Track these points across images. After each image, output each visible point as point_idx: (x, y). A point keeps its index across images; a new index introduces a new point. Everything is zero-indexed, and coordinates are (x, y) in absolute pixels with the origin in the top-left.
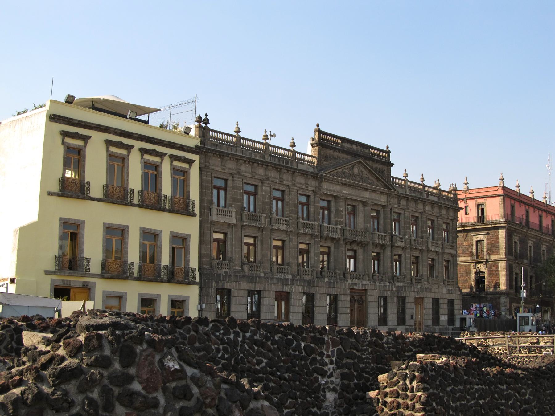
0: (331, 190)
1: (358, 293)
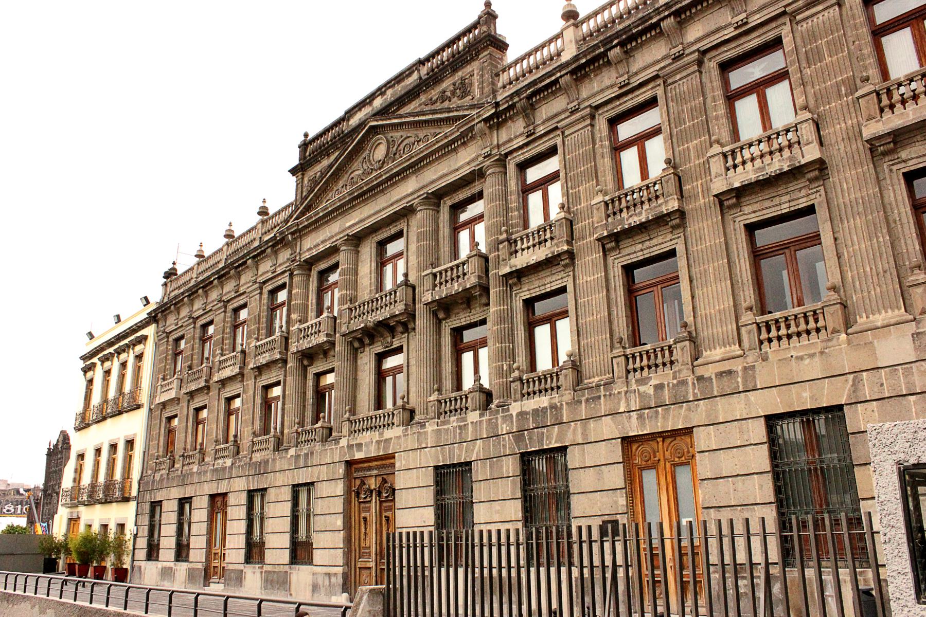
1: (378, 467)
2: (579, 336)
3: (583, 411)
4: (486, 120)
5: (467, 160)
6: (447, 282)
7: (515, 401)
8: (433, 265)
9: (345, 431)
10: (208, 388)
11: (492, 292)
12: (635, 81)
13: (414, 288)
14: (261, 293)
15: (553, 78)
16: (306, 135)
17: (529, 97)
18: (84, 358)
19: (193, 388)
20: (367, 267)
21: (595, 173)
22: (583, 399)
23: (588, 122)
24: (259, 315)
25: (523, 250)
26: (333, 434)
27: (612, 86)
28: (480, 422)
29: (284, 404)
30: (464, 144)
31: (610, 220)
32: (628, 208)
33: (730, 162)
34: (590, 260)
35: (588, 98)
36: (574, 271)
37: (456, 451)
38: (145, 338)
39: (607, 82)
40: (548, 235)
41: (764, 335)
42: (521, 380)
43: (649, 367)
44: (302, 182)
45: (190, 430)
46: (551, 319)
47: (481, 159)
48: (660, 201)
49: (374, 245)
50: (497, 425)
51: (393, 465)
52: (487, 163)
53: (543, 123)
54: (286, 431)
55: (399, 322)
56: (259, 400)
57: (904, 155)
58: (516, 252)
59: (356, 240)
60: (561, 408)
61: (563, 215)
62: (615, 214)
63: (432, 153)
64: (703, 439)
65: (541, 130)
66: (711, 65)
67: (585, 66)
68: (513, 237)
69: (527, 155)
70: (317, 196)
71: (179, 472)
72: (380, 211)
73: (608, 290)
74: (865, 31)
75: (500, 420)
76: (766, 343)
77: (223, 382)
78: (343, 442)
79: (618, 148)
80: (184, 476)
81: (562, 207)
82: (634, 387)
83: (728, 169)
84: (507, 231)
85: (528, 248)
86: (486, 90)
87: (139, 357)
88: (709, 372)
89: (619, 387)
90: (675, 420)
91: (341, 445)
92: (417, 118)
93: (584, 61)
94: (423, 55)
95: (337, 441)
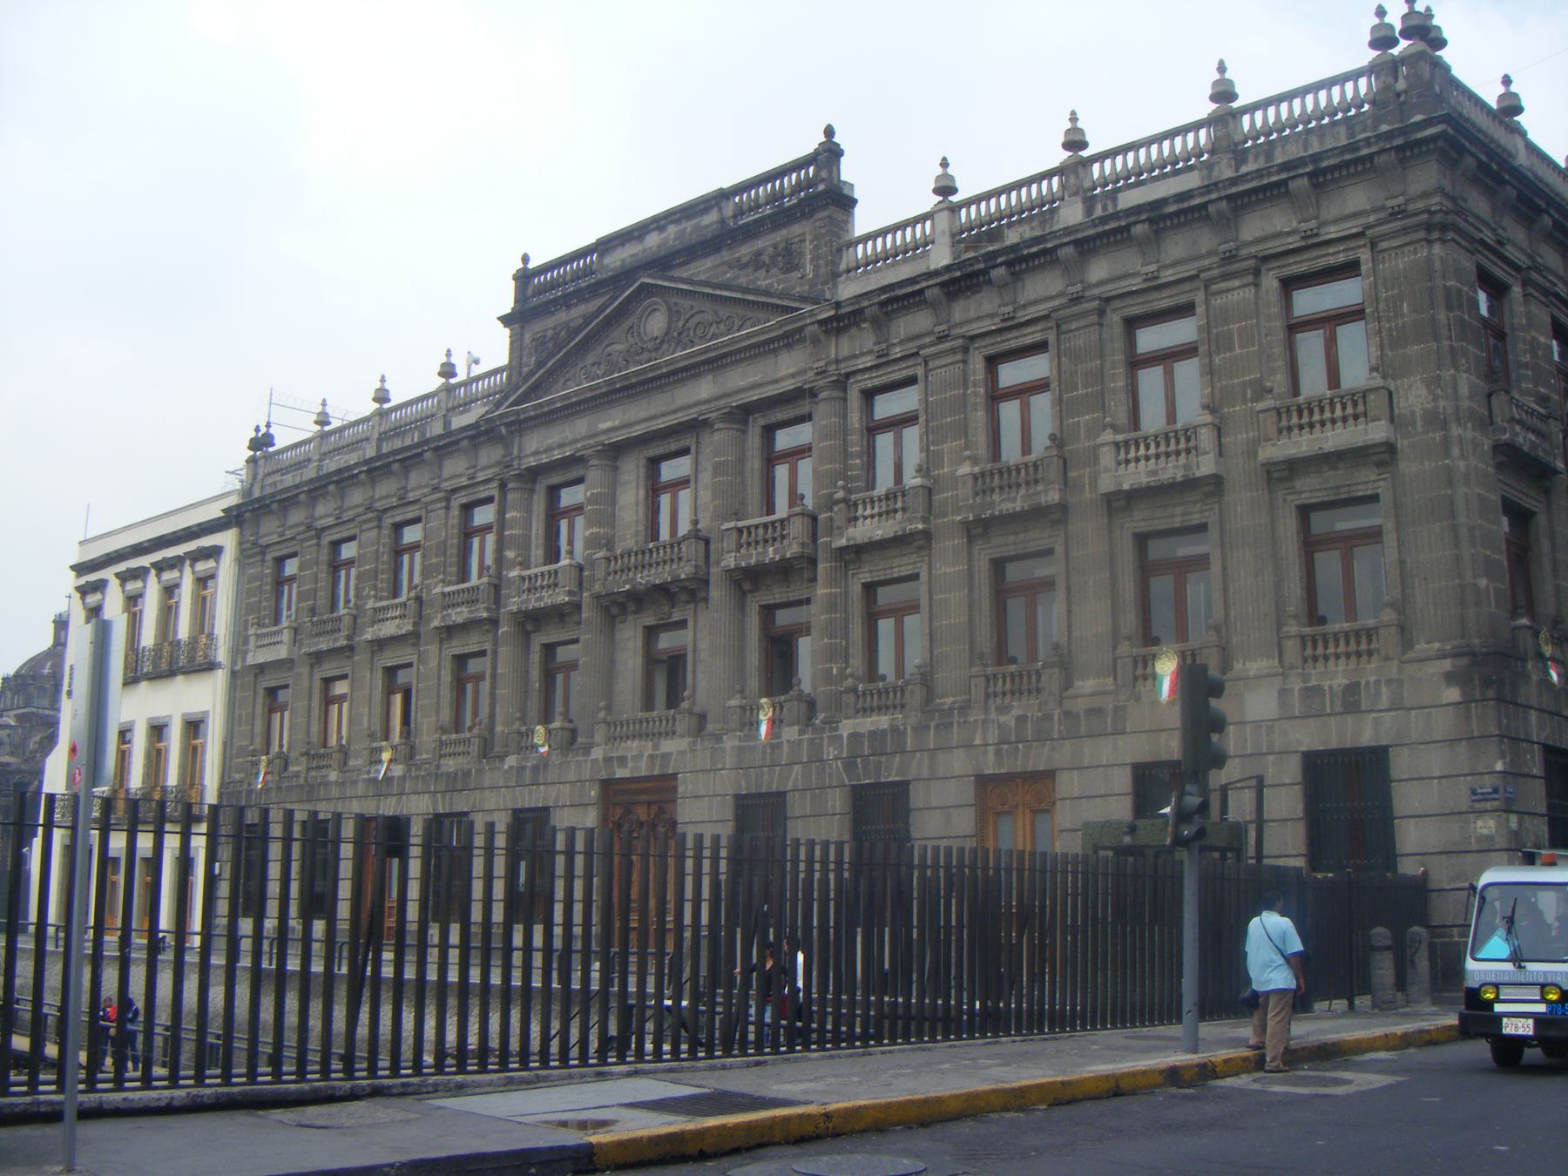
0: (549, 450)
2: (931, 640)
3: (931, 739)
4: (820, 322)
5: (791, 371)
6: (757, 542)
7: (847, 718)
8: (738, 516)
9: (600, 735)
10: (351, 648)
11: (821, 566)
12: (1023, 316)
13: (707, 542)
14: (447, 508)
15: (917, 287)
16: (525, 259)
17: (882, 304)
18: (80, 569)
19: (324, 647)
20: (631, 496)
21: (963, 430)
22: (933, 724)
23: (959, 357)
24: (445, 542)
25: (865, 518)
26: (580, 740)
27: (992, 316)
28: (800, 741)
29: (493, 687)
30: (789, 346)
31: (978, 500)
32: (1001, 488)
33: (1122, 456)
34: (949, 545)
35: (961, 324)
36: (930, 556)
37: (766, 777)
38: (215, 552)
39: (987, 308)
40: (899, 505)
41: (1309, 652)
42: (854, 690)
43: (1013, 693)
44: (522, 339)
45: (316, 713)
46: (899, 612)
47: (811, 374)
48: (1040, 488)
49: (643, 462)
50: (821, 746)
51: (675, 789)
52: (821, 383)
53: (901, 343)
54: (499, 729)
55: (684, 589)
56: (447, 676)
57: (1298, 484)
58: (856, 519)
59: (615, 452)
60: (905, 733)
61: (918, 481)
62: (984, 492)
63: (740, 351)
64: (1068, 784)
65: (897, 352)
66: (1114, 318)
67: (961, 281)
68: (853, 497)
69: (877, 382)
70: (550, 373)
71: (302, 781)
72: (655, 417)
73: (971, 589)
74: (1278, 325)
75: (826, 741)
76: (1310, 662)
77: (380, 644)
78: (597, 753)
79: (996, 397)
80: (312, 787)
81: (919, 470)
82: (993, 715)
83: (1119, 463)
84: (844, 488)
85: (872, 516)
86: (822, 271)
87: (203, 581)
88: (1080, 706)
89: (975, 715)
90: (1038, 760)
91: (592, 757)
92: (718, 292)
93: (958, 274)
94: (727, 183)
95: (587, 749)
